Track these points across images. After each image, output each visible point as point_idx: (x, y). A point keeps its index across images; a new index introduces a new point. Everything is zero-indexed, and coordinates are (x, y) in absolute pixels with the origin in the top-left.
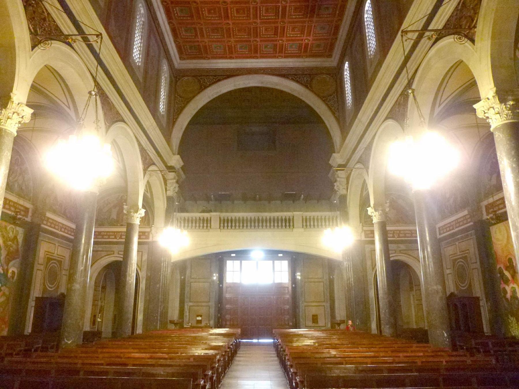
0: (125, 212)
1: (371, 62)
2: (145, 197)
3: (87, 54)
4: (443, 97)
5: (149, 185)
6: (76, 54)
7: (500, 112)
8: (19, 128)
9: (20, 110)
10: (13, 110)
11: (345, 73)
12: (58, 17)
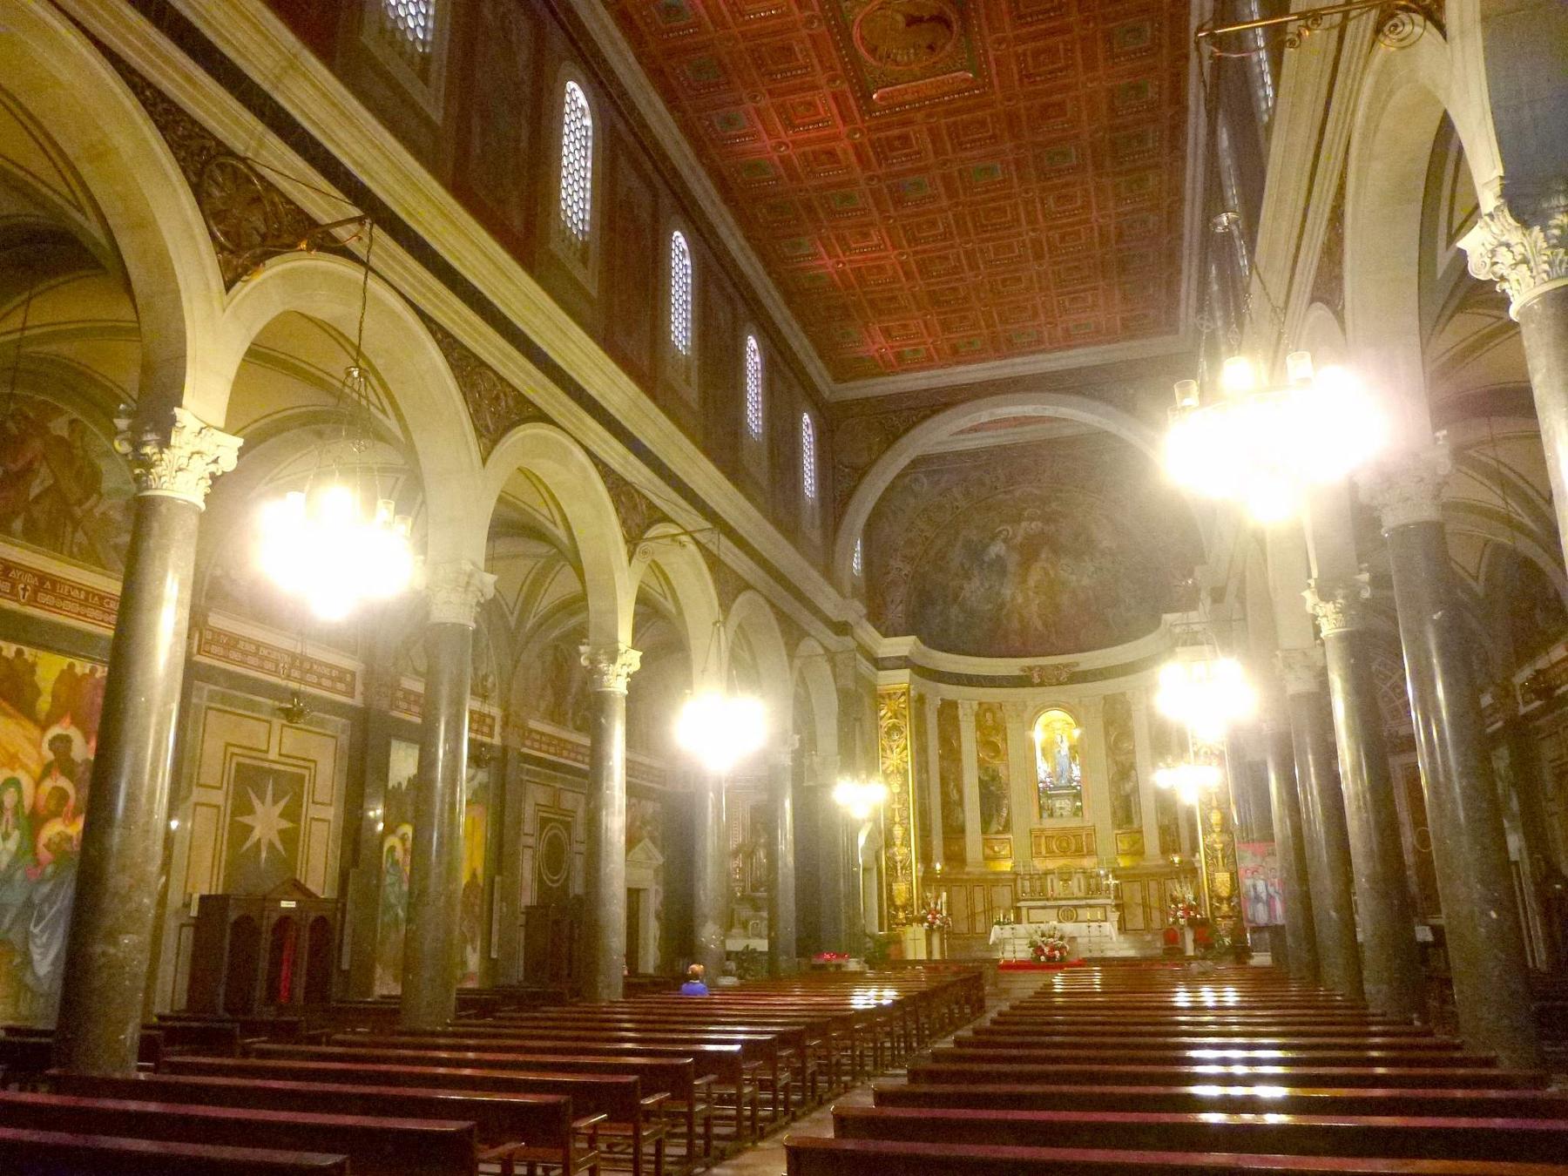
3: (401, 263)
4: (1456, 213)
7: (1530, 256)
9: (203, 447)
10: (188, 450)
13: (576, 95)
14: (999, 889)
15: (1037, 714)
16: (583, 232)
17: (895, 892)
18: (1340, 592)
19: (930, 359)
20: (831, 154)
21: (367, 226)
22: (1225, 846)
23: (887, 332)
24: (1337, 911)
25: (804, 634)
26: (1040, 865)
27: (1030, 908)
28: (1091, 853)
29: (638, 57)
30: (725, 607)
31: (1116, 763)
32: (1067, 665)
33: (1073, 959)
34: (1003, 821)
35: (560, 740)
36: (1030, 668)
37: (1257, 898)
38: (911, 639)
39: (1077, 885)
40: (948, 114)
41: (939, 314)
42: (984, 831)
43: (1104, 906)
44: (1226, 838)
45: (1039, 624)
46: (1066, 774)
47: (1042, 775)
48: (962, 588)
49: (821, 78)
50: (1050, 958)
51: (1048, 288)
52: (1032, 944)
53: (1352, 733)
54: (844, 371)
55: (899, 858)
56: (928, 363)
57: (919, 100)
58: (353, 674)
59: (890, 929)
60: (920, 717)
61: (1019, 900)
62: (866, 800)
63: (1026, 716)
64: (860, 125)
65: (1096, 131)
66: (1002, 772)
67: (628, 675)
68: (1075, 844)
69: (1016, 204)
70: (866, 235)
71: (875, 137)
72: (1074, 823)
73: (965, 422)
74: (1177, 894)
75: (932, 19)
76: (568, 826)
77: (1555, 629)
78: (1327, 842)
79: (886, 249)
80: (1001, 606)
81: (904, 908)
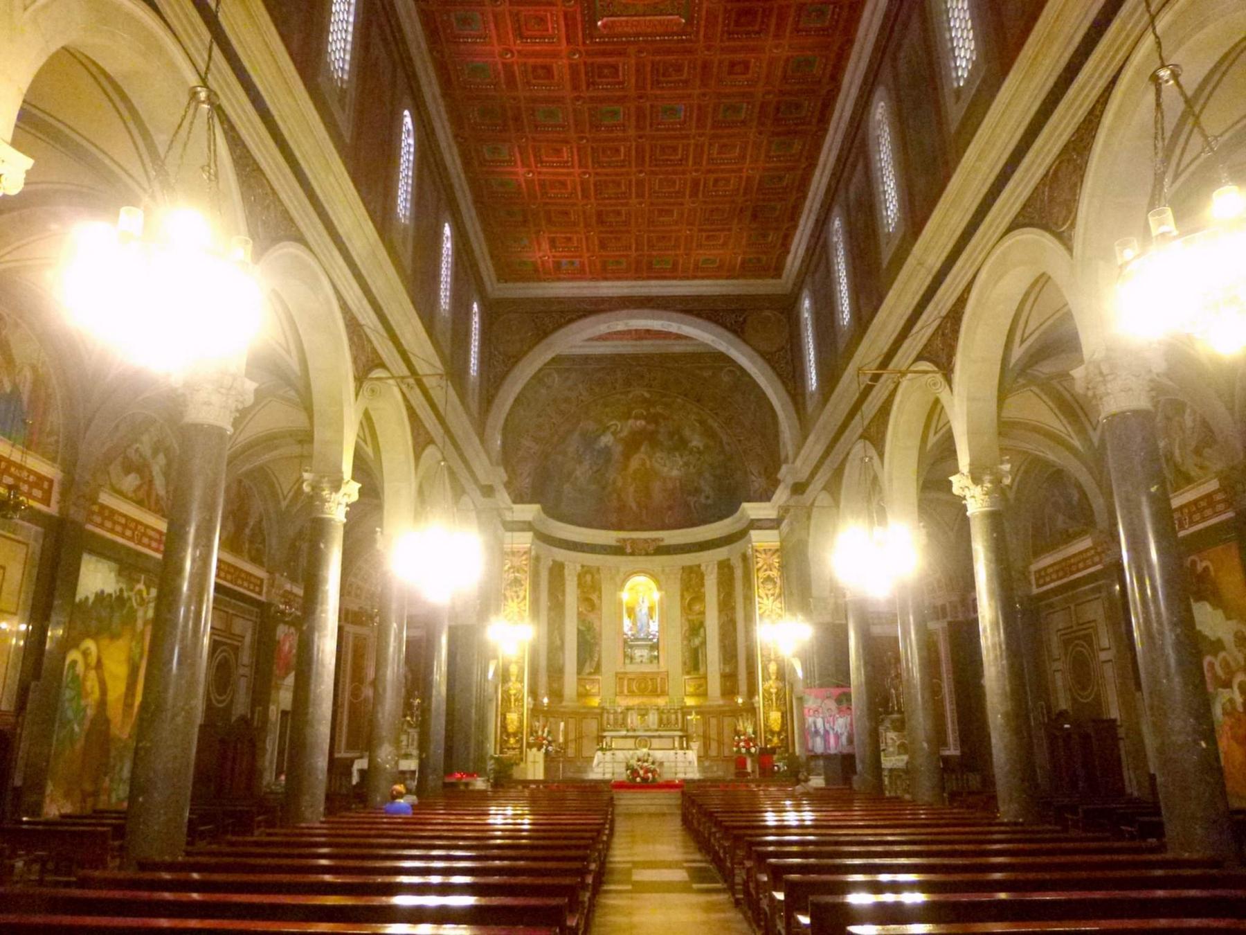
0: (306, 488)
1: (958, 93)
2: (359, 457)
5: (368, 423)
6: (158, 19)
11: (835, 239)
12: (185, 30)
14: (588, 721)
17: (508, 721)
18: (987, 478)
19: (582, 270)
20: (548, 70)
23: (552, 242)
24: (928, 742)
25: (464, 492)
27: (612, 737)
28: (663, 693)
31: (689, 621)
33: (660, 780)
34: (594, 664)
36: (624, 540)
37: (817, 732)
38: (536, 508)
39: (653, 718)
42: (579, 672)
43: (673, 737)
47: (626, 629)
50: (645, 779)
51: (692, 224)
53: (991, 593)
54: (507, 272)
55: (512, 692)
58: (51, 482)
59: (501, 752)
60: (535, 575)
63: (618, 580)
65: (769, 93)
66: (596, 625)
68: (651, 685)
70: (558, 152)
71: (589, 61)
72: (652, 668)
73: (603, 329)
74: (740, 727)
76: (236, 649)
79: (573, 167)
81: (515, 735)
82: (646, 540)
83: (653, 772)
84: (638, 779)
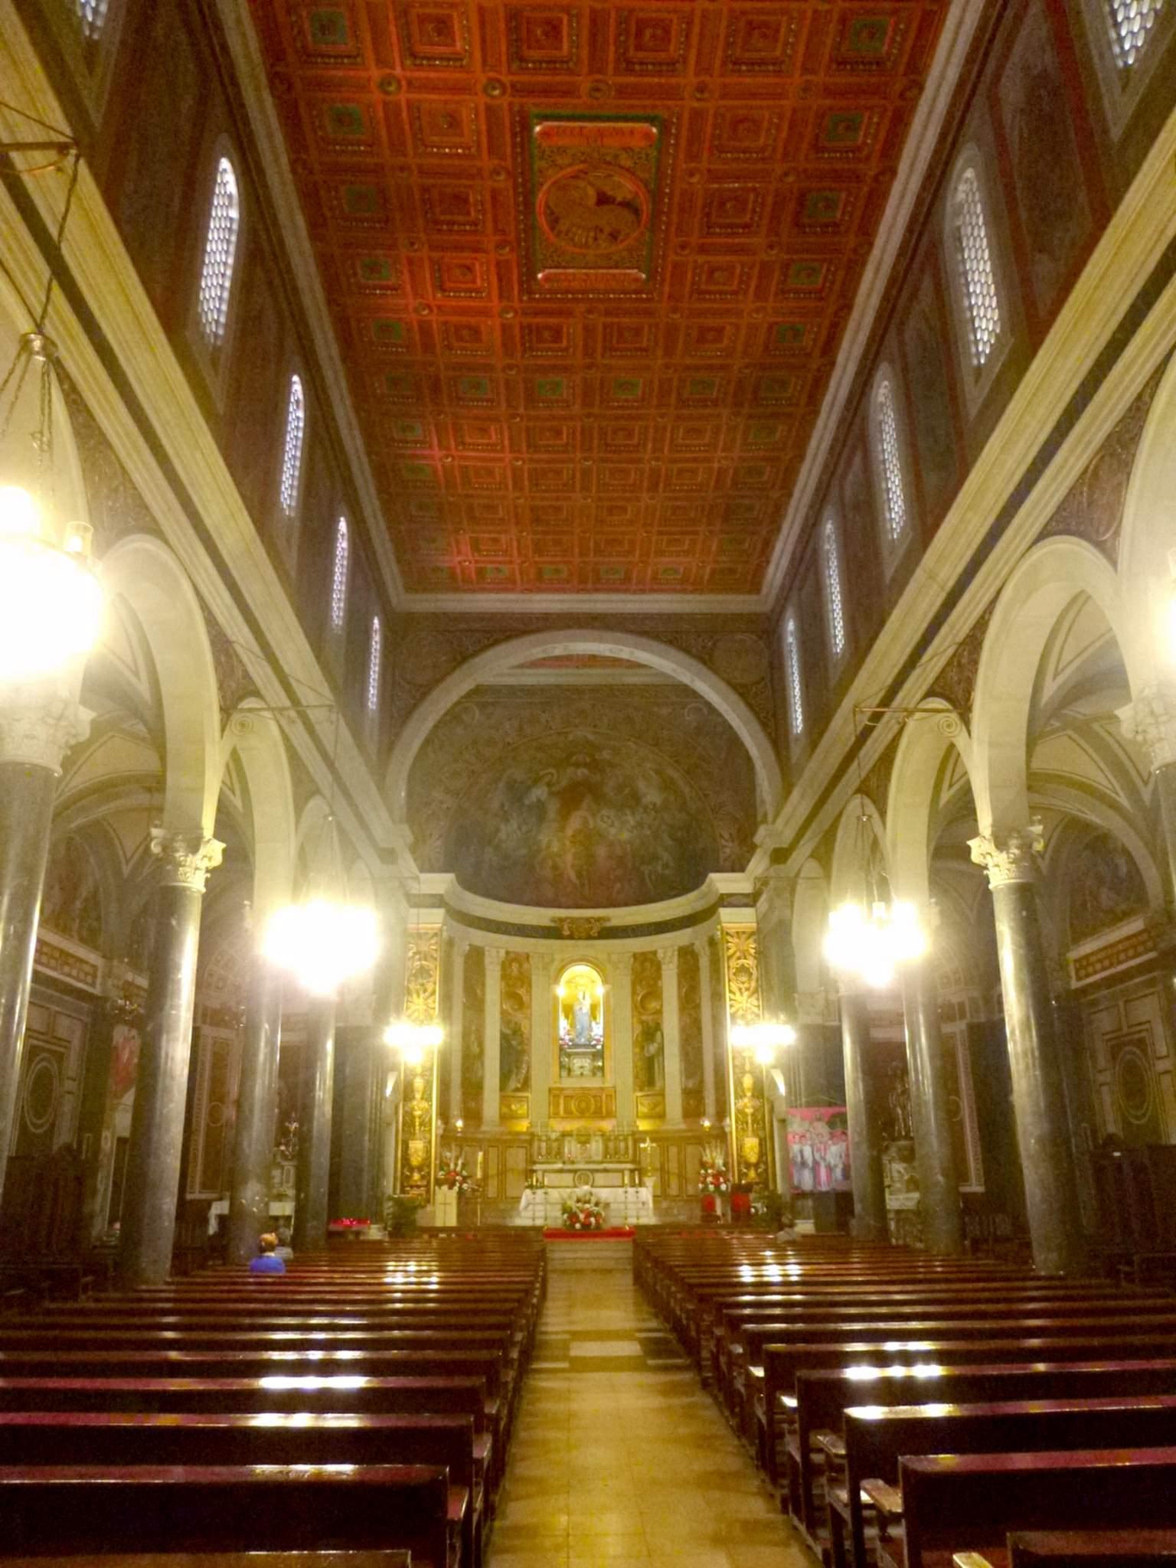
0: (155, 848)
2: (223, 809)
5: (236, 766)
8: (207, 880)
13: (227, 178)
15: (561, 970)
16: (216, 335)
17: (412, 1151)
18: (1014, 842)
20: (476, 332)
21: (71, 159)
22: (756, 1110)
23: (475, 546)
26: (558, 1126)
27: (545, 1171)
28: (610, 1115)
29: (293, 163)
30: (299, 808)
31: (642, 1022)
32: (598, 920)
33: (606, 1227)
34: (522, 1077)
35: (62, 951)
36: (561, 920)
37: (804, 1164)
39: (596, 1147)
40: (608, 313)
41: (535, 533)
42: (503, 1087)
43: (622, 1171)
44: (757, 1103)
45: (572, 875)
46: (586, 1033)
47: (562, 1033)
48: (498, 830)
49: (490, 241)
50: (586, 1226)
51: (651, 525)
52: (565, 1210)
53: (1021, 987)
54: (419, 580)
55: (418, 1113)
56: (507, 585)
57: (584, 292)
61: (535, 1163)
62: (415, 1043)
63: (553, 968)
64: (516, 304)
66: (525, 1030)
67: (207, 871)
68: (595, 1105)
69: (646, 428)
72: (594, 1083)
75: (621, 204)
76: (60, 1058)
77: (1124, 907)
78: (936, 1103)
79: (502, 450)
80: (539, 851)
81: (420, 1169)
82: (588, 920)
83: (597, 1216)
84: (578, 1226)
